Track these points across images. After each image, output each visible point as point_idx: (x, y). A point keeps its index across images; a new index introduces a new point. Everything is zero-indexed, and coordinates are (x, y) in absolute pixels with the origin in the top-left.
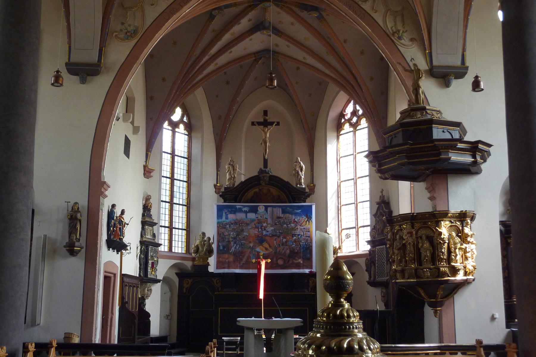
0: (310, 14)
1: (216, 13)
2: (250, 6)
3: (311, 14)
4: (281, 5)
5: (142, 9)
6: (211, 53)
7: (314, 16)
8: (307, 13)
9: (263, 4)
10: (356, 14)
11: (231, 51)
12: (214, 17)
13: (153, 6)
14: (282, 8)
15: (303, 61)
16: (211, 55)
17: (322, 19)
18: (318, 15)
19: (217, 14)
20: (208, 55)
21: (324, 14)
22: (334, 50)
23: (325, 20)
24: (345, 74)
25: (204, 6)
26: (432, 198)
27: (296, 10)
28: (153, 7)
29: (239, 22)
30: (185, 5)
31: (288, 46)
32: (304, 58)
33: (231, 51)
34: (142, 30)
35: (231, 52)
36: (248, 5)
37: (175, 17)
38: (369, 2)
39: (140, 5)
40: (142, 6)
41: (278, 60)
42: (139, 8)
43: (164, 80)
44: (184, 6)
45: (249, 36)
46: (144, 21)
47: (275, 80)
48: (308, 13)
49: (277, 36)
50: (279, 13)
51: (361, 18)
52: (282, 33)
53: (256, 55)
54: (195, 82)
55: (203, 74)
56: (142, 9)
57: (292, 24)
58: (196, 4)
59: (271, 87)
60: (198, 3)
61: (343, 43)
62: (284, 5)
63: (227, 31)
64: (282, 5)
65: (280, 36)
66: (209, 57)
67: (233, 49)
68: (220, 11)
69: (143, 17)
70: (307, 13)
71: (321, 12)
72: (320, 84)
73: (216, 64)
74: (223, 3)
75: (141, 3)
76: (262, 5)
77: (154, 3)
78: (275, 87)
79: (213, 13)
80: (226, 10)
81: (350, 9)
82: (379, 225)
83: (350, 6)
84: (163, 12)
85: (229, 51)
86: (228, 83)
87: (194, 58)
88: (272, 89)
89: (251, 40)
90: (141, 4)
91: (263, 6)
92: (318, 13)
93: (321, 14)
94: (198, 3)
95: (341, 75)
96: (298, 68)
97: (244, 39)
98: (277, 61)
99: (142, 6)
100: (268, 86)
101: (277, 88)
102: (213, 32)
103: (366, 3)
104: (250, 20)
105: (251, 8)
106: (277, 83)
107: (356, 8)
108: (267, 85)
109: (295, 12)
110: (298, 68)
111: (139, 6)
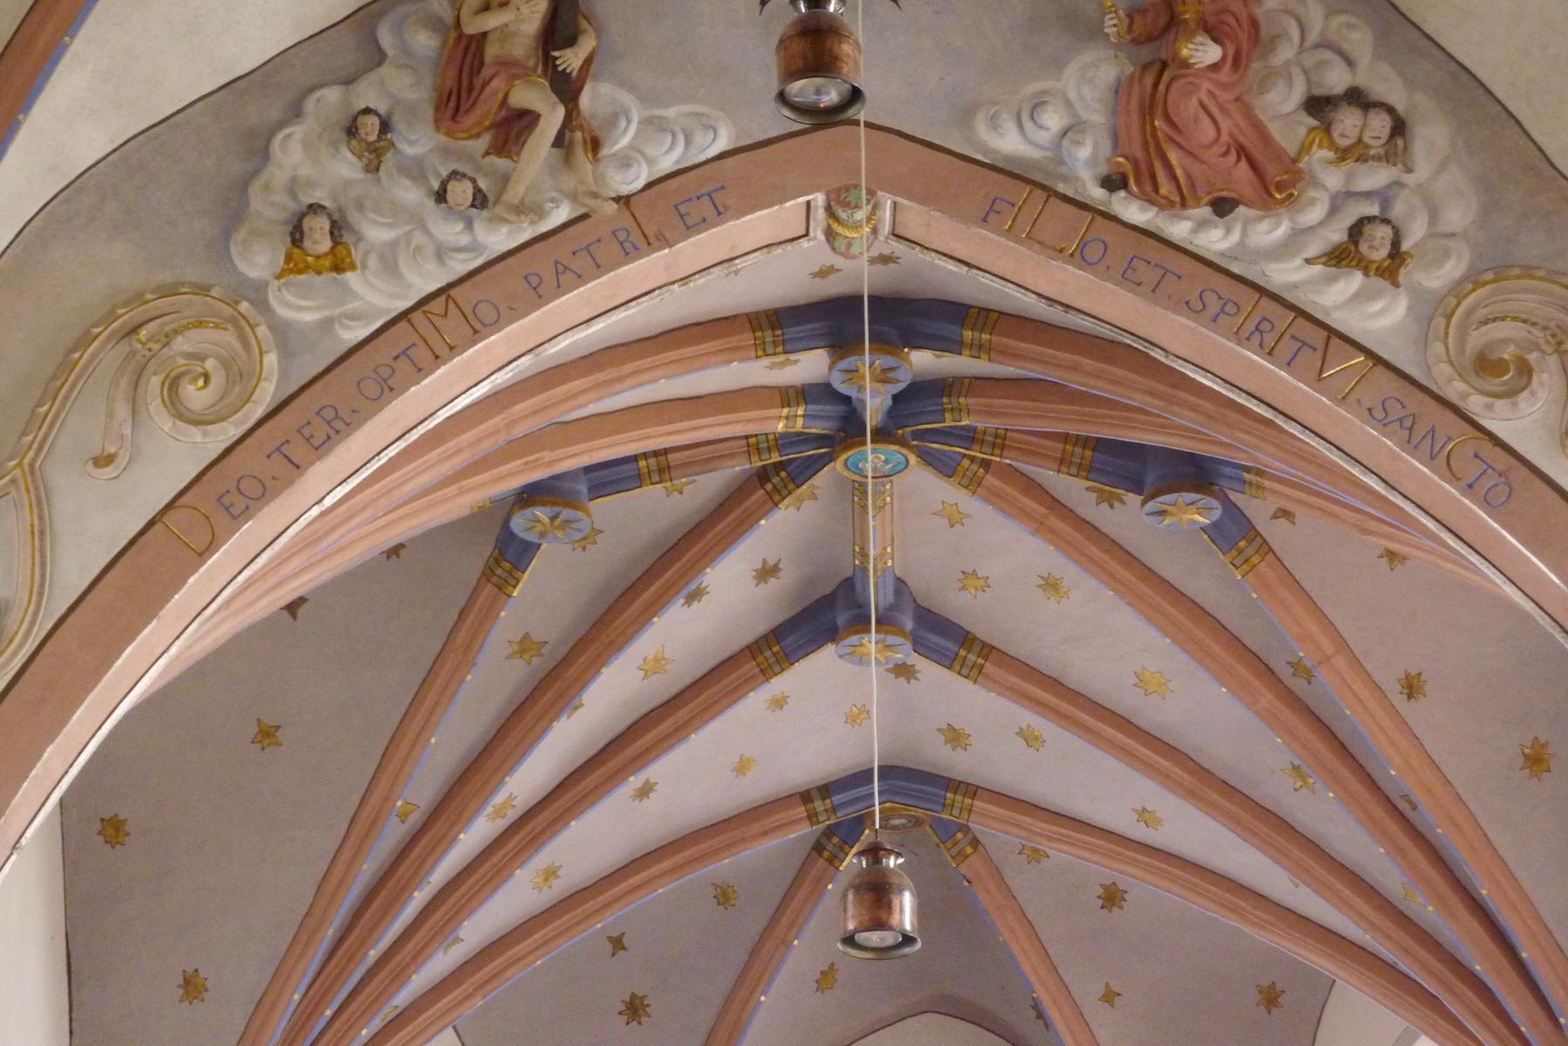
0: (1163, 513)
1: (539, 528)
2: (762, 476)
3: (1170, 508)
4: (966, 463)
5: (37, 489)
6: (511, 797)
7: (1195, 522)
8: (1144, 503)
9: (844, 457)
10: (1453, 477)
11: (647, 782)
12: (527, 550)
13: (110, 468)
14: (973, 485)
15: (1138, 832)
16: (512, 815)
17: (1242, 544)
18: (1217, 514)
19: (542, 535)
20: (489, 809)
21: (1257, 509)
22: (1343, 750)
23: (1266, 548)
24: (1426, 910)
25: (447, 468)
26: (845, 82)
27: (1073, 489)
28: (108, 472)
29: (693, 586)
30: (319, 458)
31: (1030, 738)
32: (1144, 815)
33: (647, 782)
34: (33, 623)
35: (645, 791)
36: (748, 466)
37: (251, 532)
38: (1533, 394)
39: (19, 465)
40: (32, 473)
41: (975, 843)
42: (13, 481)
43: (192, 986)
44: (312, 463)
45: (767, 673)
46: (43, 565)
47: (901, 891)
48: (1152, 505)
49: (949, 668)
50: (954, 519)
51: (1486, 504)
52: (987, 650)
53: (819, 805)
54: (402, 998)
55: (458, 940)
56: (37, 489)
57: (1051, 585)
58: (392, 451)
59: (874, 938)
60: (402, 445)
61: (1399, 701)
62: (986, 464)
63: (614, 647)
64: (972, 459)
65: (975, 674)
66: (502, 824)
67: (660, 770)
68: (567, 513)
69: (42, 539)
70: (1144, 503)
71: (1233, 496)
72: (1271, 998)
73: (551, 873)
74: (581, 453)
75: (31, 454)
76: (838, 464)
77: (112, 450)
78: (908, 940)
79: (518, 523)
80: (605, 509)
81: (1411, 446)
82: (939, 808)
83: (1408, 423)
84: (170, 506)
85: (635, 781)
86: (635, 1009)
87: (392, 834)
88: (881, 951)
89: (779, 703)
90: (26, 461)
91: (846, 473)
92: (1215, 503)
93: (1234, 513)
94: (402, 445)
95: (1403, 920)
96: (1112, 897)
97: (734, 694)
98: (969, 850)
99: (32, 473)
100: (857, 931)
101: (919, 945)
102: (522, 652)
103: (1515, 405)
104: (766, 572)
105: (769, 487)
106: (921, 912)
107: (1450, 439)
108: (851, 926)
109: (1056, 506)
110: (1112, 897)
111: (18, 472)
